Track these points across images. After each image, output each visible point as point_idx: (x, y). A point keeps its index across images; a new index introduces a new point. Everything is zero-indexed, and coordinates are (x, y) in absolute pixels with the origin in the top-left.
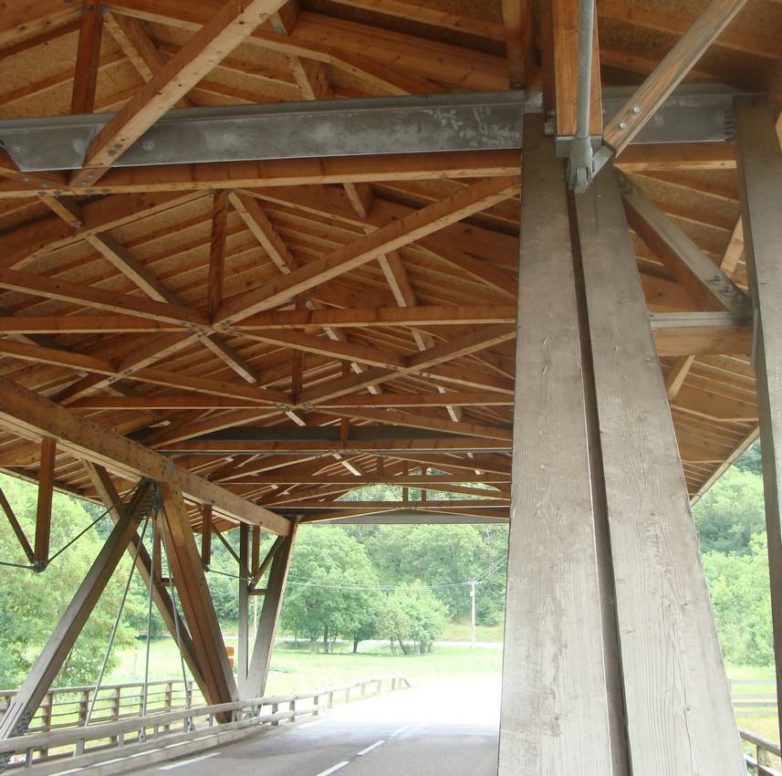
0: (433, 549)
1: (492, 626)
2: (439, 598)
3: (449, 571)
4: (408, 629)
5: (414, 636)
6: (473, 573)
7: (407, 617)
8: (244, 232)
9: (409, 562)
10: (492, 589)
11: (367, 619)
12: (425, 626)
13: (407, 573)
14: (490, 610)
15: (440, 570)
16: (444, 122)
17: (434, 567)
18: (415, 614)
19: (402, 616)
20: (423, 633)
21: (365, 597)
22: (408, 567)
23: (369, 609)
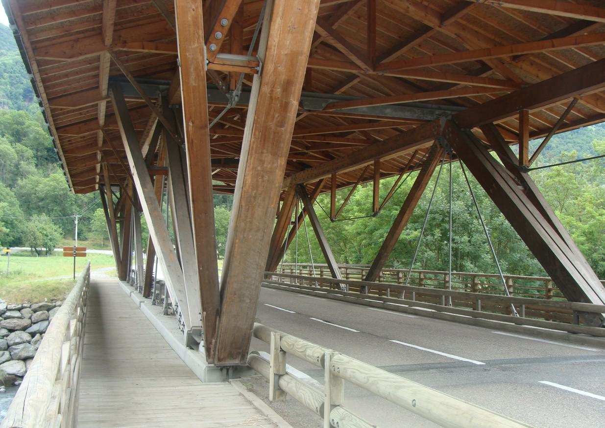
0: (51, 196)
1: (84, 240)
2: (55, 224)
3: (60, 209)
4: (41, 241)
5: (45, 245)
6: (74, 211)
7: (40, 234)
8: (33, 40)
9: (35, 203)
10: (84, 220)
11: (17, 235)
12: (51, 240)
13: (34, 209)
14: (84, 231)
15: (55, 208)
16: (417, 112)
17: (52, 206)
18: (45, 233)
19: (38, 234)
20: (50, 243)
21: (16, 222)
22: (34, 206)
23: (18, 229)
